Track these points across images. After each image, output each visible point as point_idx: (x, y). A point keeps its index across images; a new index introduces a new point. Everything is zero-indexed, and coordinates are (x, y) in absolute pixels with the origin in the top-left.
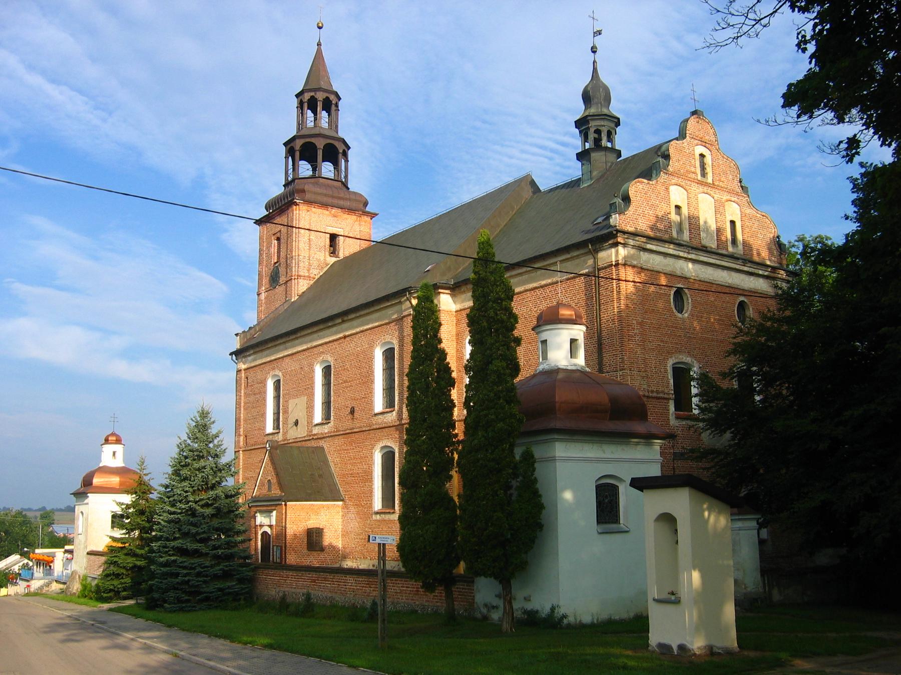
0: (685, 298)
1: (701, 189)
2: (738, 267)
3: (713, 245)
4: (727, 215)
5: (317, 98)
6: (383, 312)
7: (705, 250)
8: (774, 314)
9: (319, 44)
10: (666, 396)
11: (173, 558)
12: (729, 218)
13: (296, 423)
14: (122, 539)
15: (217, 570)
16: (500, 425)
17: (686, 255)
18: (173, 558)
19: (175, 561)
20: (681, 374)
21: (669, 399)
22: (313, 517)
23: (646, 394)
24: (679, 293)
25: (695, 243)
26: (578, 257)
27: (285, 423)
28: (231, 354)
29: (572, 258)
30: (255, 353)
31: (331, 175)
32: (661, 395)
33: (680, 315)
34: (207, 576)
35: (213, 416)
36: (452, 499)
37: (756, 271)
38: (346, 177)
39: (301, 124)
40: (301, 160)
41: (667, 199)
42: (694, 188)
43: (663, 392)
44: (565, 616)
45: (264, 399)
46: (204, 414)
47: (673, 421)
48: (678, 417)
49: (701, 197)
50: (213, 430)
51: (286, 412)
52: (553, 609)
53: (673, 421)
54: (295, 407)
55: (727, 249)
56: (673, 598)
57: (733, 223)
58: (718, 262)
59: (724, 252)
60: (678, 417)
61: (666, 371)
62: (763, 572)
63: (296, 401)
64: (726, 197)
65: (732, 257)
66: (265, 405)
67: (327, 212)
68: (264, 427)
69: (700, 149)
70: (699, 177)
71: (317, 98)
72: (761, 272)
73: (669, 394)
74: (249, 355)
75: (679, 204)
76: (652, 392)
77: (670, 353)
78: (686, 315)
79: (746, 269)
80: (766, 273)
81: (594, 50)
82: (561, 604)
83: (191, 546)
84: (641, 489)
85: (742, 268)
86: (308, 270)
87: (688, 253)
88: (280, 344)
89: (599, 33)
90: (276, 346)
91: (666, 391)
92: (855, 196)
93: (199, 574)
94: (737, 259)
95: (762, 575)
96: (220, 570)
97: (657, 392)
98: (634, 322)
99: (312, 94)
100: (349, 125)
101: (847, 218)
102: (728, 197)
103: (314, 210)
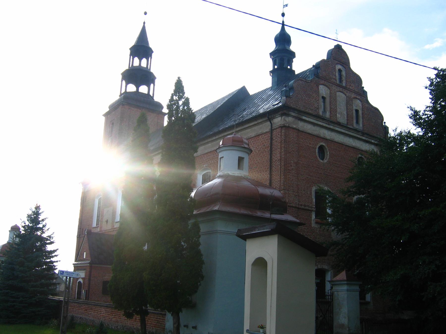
0: (325, 151)
1: (339, 89)
2: (359, 136)
4: (354, 106)
5: (142, 49)
9: (144, 23)
10: (310, 209)
11: (7, 291)
12: (355, 108)
17: (327, 126)
18: (7, 291)
21: (312, 211)
24: (321, 149)
26: (261, 123)
29: (258, 124)
32: (307, 208)
33: (322, 161)
36: (38, 225)
37: (370, 140)
38: (153, 94)
40: (365, 299)
41: (317, 92)
42: (334, 88)
43: (308, 206)
46: (38, 208)
48: (316, 223)
49: (338, 94)
50: (41, 217)
53: (313, 225)
55: (353, 126)
57: (357, 111)
58: (347, 132)
59: (351, 127)
61: (311, 194)
62: (362, 321)
64: (353, 95)
65: (356, 131)
68: (92, 224)
69: (339, 67)
70: (338, 82)
71: (142, 49)
72: (373, 141)
73: (312, 208)
75: (324, 96)
76: (301, 205)
78: (326, 161)
79: (364, 138)
80: (376, 142)
81: (283, 15)
85: (361, 137)
87: (329, 125)
91: (310, 205)
95: (361, 323)
97: (305, 206)
98: (292, 162)
100: (156, 65)
101: (426, 88)
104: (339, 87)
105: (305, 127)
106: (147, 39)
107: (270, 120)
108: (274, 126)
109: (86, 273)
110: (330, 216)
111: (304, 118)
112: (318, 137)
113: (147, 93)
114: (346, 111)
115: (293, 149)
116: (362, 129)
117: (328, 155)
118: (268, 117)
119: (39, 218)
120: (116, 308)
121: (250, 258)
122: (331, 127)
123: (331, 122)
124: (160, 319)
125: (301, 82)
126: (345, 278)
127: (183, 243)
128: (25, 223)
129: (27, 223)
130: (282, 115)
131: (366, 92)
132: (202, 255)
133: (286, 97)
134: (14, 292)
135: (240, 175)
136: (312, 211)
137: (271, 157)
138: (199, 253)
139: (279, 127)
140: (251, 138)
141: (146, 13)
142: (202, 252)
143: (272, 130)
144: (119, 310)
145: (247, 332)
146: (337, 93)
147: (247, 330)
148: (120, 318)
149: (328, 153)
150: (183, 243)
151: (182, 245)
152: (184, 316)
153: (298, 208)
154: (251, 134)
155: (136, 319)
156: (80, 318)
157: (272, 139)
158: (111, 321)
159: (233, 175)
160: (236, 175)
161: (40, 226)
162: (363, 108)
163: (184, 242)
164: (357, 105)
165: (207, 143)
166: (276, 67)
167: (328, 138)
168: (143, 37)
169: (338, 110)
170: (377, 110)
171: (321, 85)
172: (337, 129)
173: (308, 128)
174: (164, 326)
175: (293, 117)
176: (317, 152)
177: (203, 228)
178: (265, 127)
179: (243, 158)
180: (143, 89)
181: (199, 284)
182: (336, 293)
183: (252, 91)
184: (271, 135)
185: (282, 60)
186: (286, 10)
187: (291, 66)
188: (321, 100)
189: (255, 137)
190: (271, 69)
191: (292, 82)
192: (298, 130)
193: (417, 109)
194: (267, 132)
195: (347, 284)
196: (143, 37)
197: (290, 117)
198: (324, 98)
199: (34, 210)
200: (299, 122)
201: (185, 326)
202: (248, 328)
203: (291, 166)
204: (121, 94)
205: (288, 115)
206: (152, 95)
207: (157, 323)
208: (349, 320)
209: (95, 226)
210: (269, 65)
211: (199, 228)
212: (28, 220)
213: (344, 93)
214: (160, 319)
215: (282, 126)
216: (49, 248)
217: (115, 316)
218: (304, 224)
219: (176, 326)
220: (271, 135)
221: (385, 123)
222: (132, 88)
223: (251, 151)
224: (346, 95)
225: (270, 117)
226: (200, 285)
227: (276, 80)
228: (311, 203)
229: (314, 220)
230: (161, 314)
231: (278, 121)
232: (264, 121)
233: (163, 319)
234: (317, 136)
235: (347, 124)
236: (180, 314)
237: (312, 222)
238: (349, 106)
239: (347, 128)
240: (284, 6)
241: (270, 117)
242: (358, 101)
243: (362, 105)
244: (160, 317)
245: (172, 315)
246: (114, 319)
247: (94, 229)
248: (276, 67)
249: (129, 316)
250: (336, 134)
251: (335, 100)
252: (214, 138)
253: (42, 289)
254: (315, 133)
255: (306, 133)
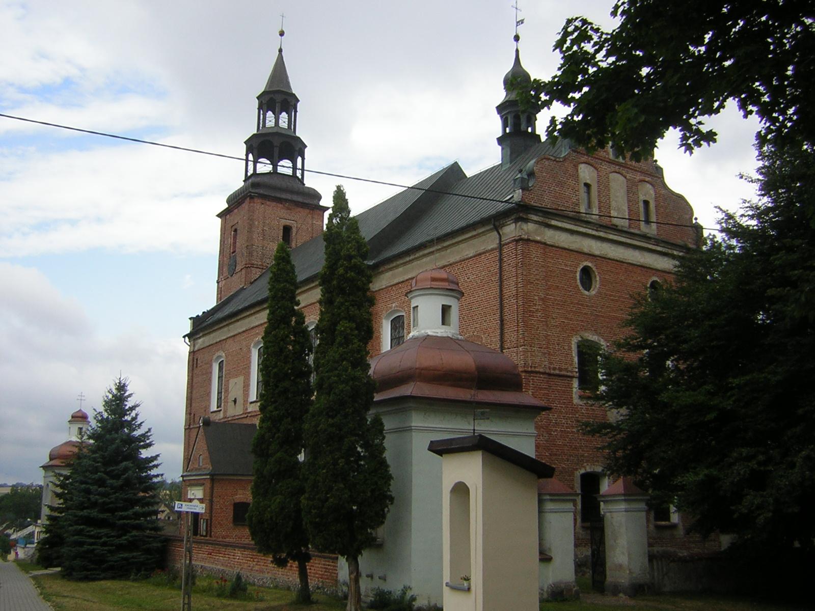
0: (593, 276)
2: (650, 246)
3: (623, 224)
6: (310, 293)
7: (615, 229)
8: (671, 286)
9: (280, 51)
10: (569, 374)
11: (82, 527)
13: (235, 401)
14: (59, 508)
15: (124, 540)
16: (341, 387)
18: (82, 527)
19: (82, 530)
20: (587, 353)
21: (573, 377)
22: (240, 492)
23: (548, 371)
25: (605, 221)
27: (226, 402)
28: (184, 337)
29: (478, 235)
30: (203, 336)
31: (289, 172)
32: (562, 373)
33: (586, 293)
34: (112, 545)
35: (130, 390)
39: (261, 121)
41: (576, 177)
43: (566, 370)
44: (413, 599)
45: (210, 380)
46: (121, 387)
47: (576, 400)
50: (129, 404)
51: (227, 391)
52: (404, 593)
53: (576, 400)
54: (235, 387)
56: (466, 584)
57: (646, 203)
58: (629, 241)
60: (581, 397)
61: (570, 348)
62: (651, 558)
63: (235, 380)
64: (639, 177)
65: (645, 237)
66: (210, 384)
67: (281, 205)
72: (675, 253)
73: (572, 372)
74: (200, 338)
75: (588, 182)
76: (554, 369)
77: (574, 331)
78: (594, 293)
79: (659, 249)
81: (517, 38)
82: (413, 585)
83: (94, 513)
84: (440, 453)
85: (654, 247)
86: (262, 259)
87: (597, 231)
88: (224, 326)
89: (522, 22)
90: (221, 328)
91: (570, 369)
92: (760, 164)
93: (104, 544)
94: (650, 238)
96: (126, 540)
97: (560, 369)
98: (536, 298)
99: (272, 96)
102: (642, 178)
103: (268, 203)
104: (614, 164)
105: (556, 237)
106: (287, 77)
107: (497, 228)
108: (505, 239)
109: (204, 491)
110: (602, 382)
111: (553, 223)
112: (580, 253)
113: (300, 278)
114: (626, 205)
115: (538, 277)
116: (655, 232)
117: (598, 282)
118: (494, 225)
119: (126, 405)
120: (260, 552)
121: (447, 485)
122: (602, 234)
123: (601, 226)
124: (329, 565)
125: (547, 163)
126: (622, 491)
127: (359, 449)
128: (102, 416)
129: (105, 415)
130: (517, 220)
131: (662, 169)
132: (388, 466)
133: (523, 189)
134: (92, 529)
135: (445, 335)
136: (573, 377)
137: (501, 291)
138: (383, 464)
139: (513, 241)
140: (467, 259)
141: (282, 34)
142: (389, 462)
143: (501, 246)
144: (264, 555)
145: (446, 586)
146: (611, 174)
147: (447, 583)
148: (267, 566)
149: (598, 279)
150: (359, 449)
151: (359, 452)
152: (365, 560)
153: (549, 374)
154: (467, 253)
155: (291, 566)
156: (202, 566)
157: (501, 260)
158: (252, 570)
159: (434, 334)
160: (439, 335)
161: (128, 418)
162: (656, 198)
163: (361, 447)
164: (647, 192)
165: (397, 267)
166: (508, 130)
167: (597, 253)
168: (279, 72)
169: (613, 204)
170: (680, 198)
171: (582, 163)
172: (611, 237)
173: (563, 239)
174: (337, 577)
175: (536, 222)
176: (578, 277)
177: (389, 423)
178: (490, 241)
179: (450, 306)
180: (285, 166)
181: (386, 509)
182: (608, 514)
183: (470, 172)
184: (501, 254)
185: (517, 118)
186: (521, 31)
187: (534, 129)
188: (583, 189)
189: (474, 256)
190: (500, 134)
191: (532, 162)
192: (545, 244)
193: (731, 212)
194: (492, 250)
195: (625, 500)
196: (279, 72)
197: (529, 224)
198: (587, 186)
199: (115, 392)
200: (546, 229)
201: (368, 576)
202: (448, 581)
203: (535, 305)
204: (247, 178)
205: (526, 220)
206: (300, 177)
207: (325, 572)
208: (629, 558)
209: (215, 409)
210: (495, 126)
211: (382, 424)
212: (106, 410)
213: (622, 174)
214: (329, 565)
215: (517, 238)
216: (145, 454)
217: (258, 562)
218: (548, 409)
219: (353, 576)
220: (501, 254)
221: (696, 219)
222: (264, 167)
223: (462, 294)
224: (625, 177)
225: (497, 224)
226: (388, 511)
227: (509, 153)
228: (571, 365)
229: (576, 393)
230: (330, 558)
231: (511, 230)
232: (487, 231)
233: (334, 566)
234: (577, 252)
235: (630, 227)
236: (360, 559)
237: (574, 396)
238: (631, 195)
239: (629, 236)
240: (518, 22)
241: (497, 224)
242: (648, 186)
243: (655, 192)
244: (329, 562)
245: (347, 560)
246: (257, 568)
247: (214, 414)
248: (508, 130)
249: (281, 563)
250: (609, 245)
251: (607, 187)
252: (408, 259)
253: (137, 522)
254: (574, 246)
255: (557, 247)
